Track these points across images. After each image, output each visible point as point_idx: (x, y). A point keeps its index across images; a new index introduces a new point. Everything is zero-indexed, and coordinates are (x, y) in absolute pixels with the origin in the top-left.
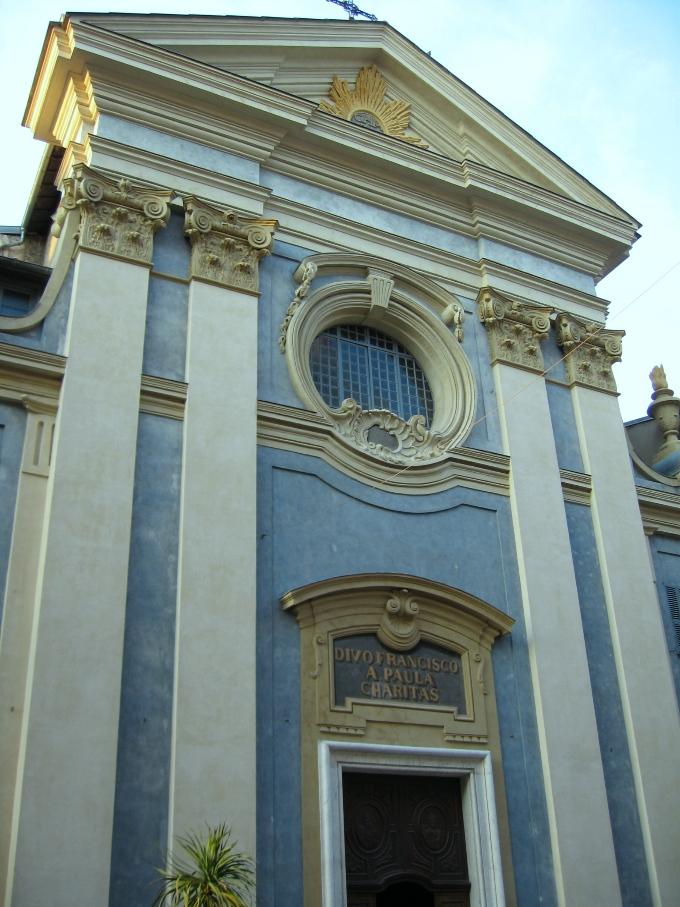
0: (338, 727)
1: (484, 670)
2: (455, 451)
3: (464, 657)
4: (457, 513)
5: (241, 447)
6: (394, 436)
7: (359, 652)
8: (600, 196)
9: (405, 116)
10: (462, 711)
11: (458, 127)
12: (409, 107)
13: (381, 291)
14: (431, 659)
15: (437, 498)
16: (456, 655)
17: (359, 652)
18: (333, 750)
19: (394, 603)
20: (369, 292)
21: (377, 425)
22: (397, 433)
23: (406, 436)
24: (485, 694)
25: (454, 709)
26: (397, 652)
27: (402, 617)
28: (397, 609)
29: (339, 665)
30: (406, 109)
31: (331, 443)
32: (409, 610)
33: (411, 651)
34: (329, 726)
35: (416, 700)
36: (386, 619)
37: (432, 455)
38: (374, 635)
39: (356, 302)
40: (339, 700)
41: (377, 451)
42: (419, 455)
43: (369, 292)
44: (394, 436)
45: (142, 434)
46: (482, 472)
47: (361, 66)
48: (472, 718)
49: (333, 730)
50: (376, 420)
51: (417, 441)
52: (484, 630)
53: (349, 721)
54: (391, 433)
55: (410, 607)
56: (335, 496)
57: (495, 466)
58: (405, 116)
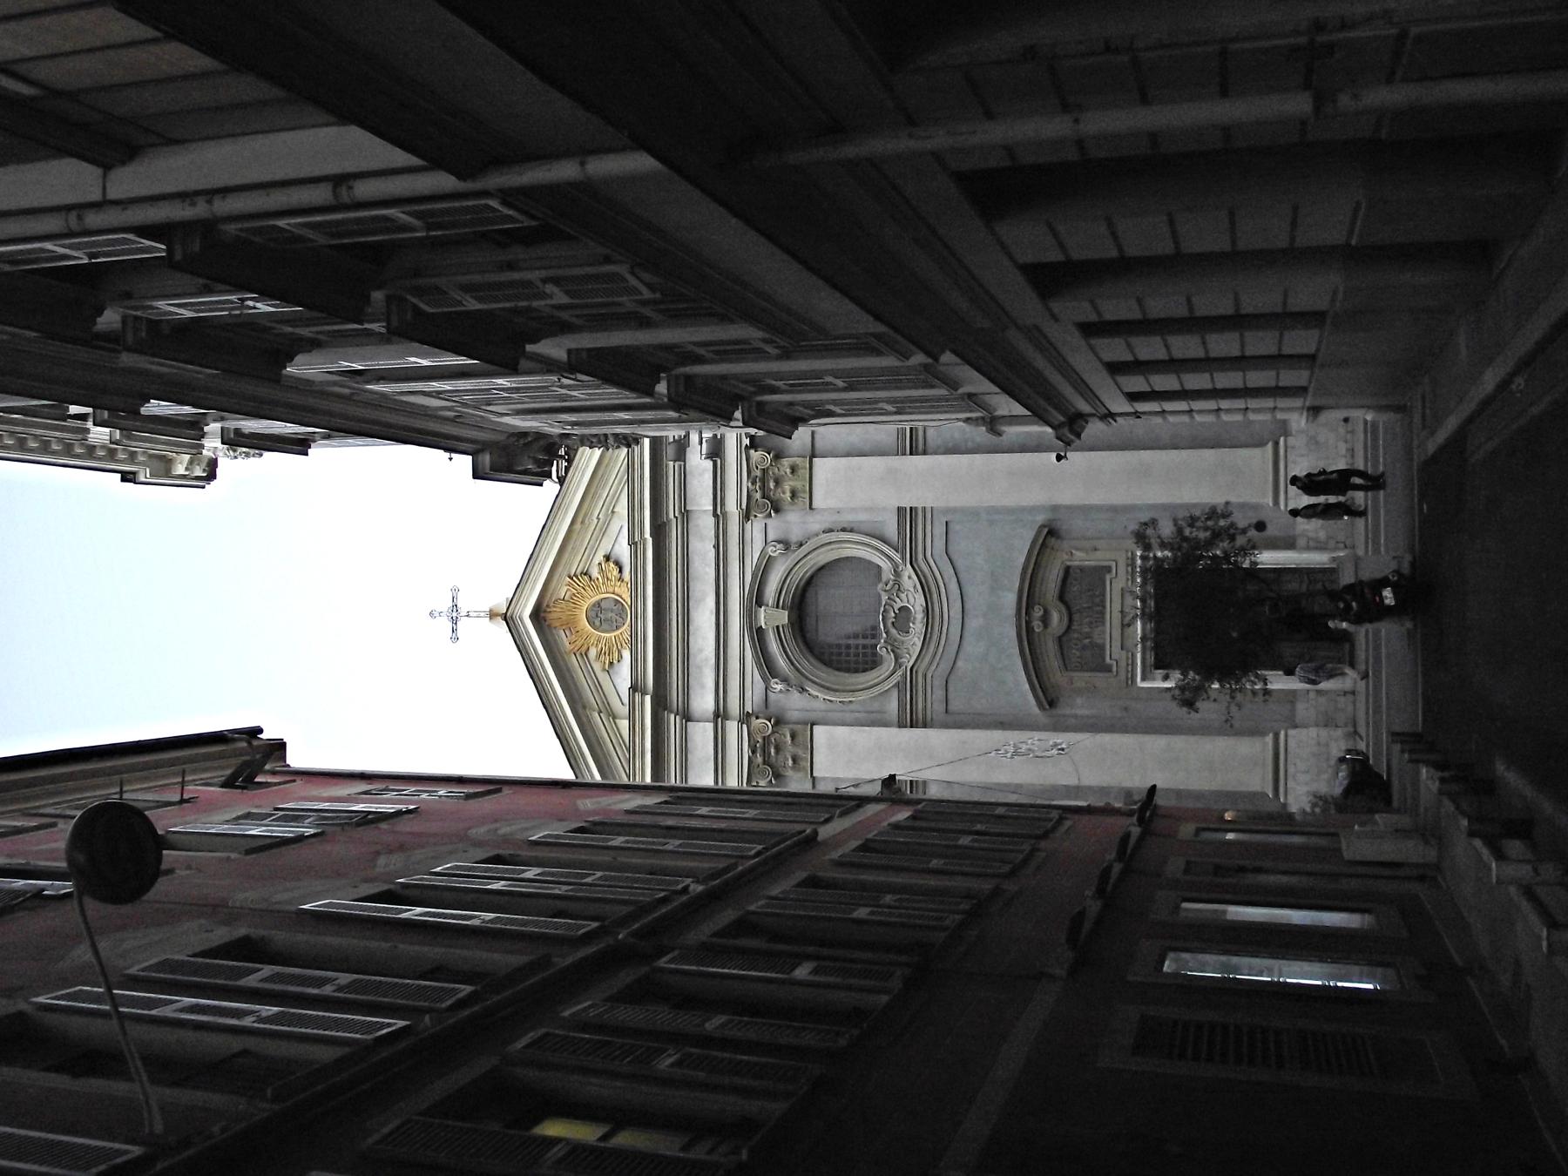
0: (1128, 671)
1: (1077, 549)
2: (903, 558)
3: (1068, 563)
4: (954, 558)
5: (938, 739)
6: (899, 609)
7: (1074, 651)
8: (540, 541)
9: (579, 579)
10: (1108, 569)
11: (569, 352)
12: (570, 577)
13: (772, 618)
14: (1074, 589)
15: (945, 577)
16: (1067, 570)
17: (1074, 651)
18: (1143, 679)
19: (1037, 626)
20: (778, 627)
21: (893, 623)
22: (896, 607)
23: (897, 599)
24: (1096, 550)
25: (1108, 577)
26: (1069, 627)
27: (1045, 620)
28: (1040, 623)
29: (1082, 668)
30: (572, 579)
31: (918, 667)
32: (1041, 613)
33: (1068, 608)
34: (1127, 679)
35: (1104, 607)
36: (1049, 630)
37: (910, 577)
38: (1060, 638)
39: (787, 635)
40: (1108, 669)
41: (917, 627)
42: (912, 590)
43: (778, 627)
44: (899, 609)
45: (931, 454)
46: (916, 691)
47: (546, 628)
48: (1114, 563)
49: (1130, 662)
50: (890, 625)
51: (899, 590)
52: (1047, 547)
53: (1123, 664)
54: (897, 612)
55: (1038, 612)
56: (960, 663)
57: (908, 711)
58: (579, 579)
